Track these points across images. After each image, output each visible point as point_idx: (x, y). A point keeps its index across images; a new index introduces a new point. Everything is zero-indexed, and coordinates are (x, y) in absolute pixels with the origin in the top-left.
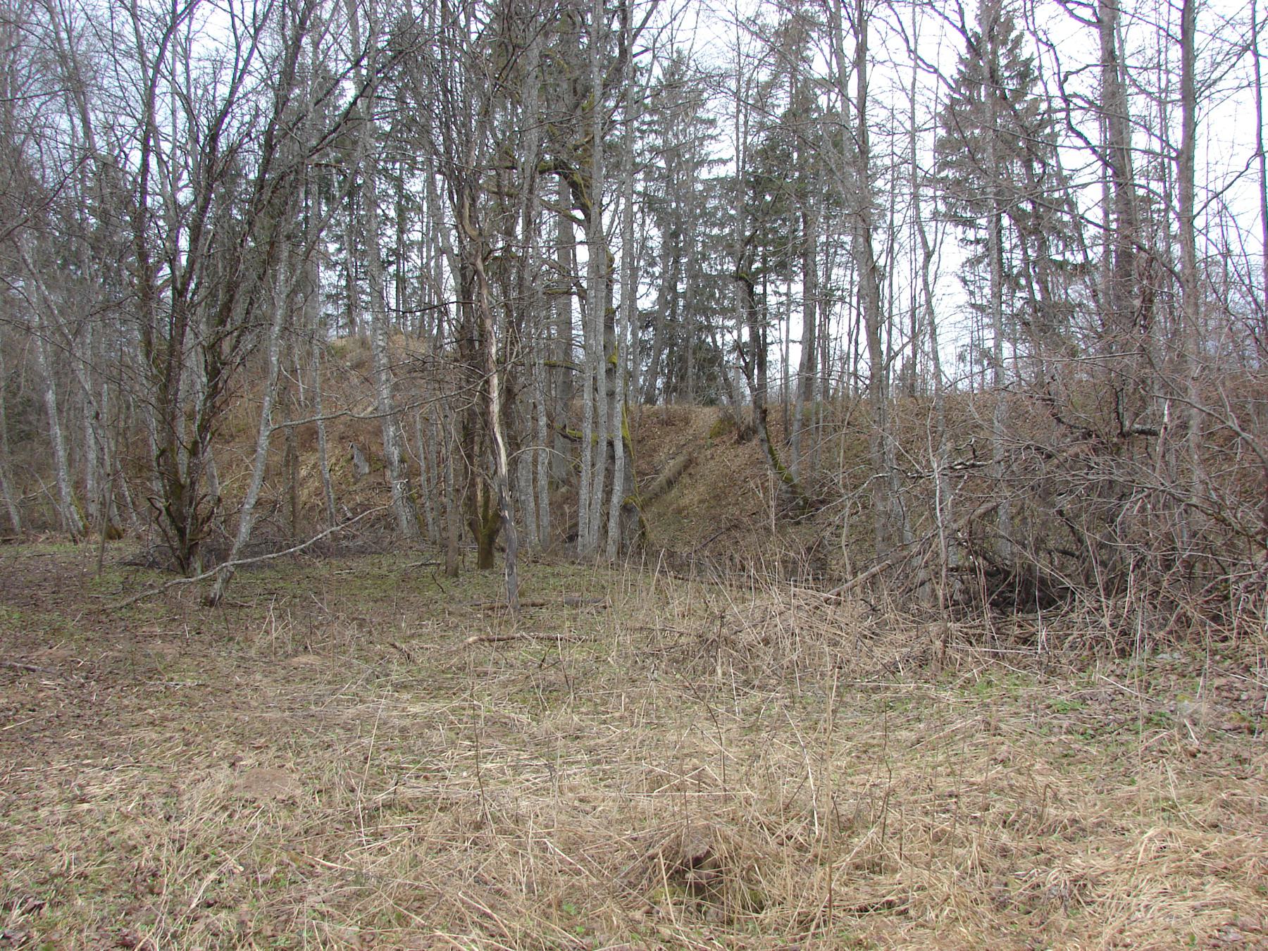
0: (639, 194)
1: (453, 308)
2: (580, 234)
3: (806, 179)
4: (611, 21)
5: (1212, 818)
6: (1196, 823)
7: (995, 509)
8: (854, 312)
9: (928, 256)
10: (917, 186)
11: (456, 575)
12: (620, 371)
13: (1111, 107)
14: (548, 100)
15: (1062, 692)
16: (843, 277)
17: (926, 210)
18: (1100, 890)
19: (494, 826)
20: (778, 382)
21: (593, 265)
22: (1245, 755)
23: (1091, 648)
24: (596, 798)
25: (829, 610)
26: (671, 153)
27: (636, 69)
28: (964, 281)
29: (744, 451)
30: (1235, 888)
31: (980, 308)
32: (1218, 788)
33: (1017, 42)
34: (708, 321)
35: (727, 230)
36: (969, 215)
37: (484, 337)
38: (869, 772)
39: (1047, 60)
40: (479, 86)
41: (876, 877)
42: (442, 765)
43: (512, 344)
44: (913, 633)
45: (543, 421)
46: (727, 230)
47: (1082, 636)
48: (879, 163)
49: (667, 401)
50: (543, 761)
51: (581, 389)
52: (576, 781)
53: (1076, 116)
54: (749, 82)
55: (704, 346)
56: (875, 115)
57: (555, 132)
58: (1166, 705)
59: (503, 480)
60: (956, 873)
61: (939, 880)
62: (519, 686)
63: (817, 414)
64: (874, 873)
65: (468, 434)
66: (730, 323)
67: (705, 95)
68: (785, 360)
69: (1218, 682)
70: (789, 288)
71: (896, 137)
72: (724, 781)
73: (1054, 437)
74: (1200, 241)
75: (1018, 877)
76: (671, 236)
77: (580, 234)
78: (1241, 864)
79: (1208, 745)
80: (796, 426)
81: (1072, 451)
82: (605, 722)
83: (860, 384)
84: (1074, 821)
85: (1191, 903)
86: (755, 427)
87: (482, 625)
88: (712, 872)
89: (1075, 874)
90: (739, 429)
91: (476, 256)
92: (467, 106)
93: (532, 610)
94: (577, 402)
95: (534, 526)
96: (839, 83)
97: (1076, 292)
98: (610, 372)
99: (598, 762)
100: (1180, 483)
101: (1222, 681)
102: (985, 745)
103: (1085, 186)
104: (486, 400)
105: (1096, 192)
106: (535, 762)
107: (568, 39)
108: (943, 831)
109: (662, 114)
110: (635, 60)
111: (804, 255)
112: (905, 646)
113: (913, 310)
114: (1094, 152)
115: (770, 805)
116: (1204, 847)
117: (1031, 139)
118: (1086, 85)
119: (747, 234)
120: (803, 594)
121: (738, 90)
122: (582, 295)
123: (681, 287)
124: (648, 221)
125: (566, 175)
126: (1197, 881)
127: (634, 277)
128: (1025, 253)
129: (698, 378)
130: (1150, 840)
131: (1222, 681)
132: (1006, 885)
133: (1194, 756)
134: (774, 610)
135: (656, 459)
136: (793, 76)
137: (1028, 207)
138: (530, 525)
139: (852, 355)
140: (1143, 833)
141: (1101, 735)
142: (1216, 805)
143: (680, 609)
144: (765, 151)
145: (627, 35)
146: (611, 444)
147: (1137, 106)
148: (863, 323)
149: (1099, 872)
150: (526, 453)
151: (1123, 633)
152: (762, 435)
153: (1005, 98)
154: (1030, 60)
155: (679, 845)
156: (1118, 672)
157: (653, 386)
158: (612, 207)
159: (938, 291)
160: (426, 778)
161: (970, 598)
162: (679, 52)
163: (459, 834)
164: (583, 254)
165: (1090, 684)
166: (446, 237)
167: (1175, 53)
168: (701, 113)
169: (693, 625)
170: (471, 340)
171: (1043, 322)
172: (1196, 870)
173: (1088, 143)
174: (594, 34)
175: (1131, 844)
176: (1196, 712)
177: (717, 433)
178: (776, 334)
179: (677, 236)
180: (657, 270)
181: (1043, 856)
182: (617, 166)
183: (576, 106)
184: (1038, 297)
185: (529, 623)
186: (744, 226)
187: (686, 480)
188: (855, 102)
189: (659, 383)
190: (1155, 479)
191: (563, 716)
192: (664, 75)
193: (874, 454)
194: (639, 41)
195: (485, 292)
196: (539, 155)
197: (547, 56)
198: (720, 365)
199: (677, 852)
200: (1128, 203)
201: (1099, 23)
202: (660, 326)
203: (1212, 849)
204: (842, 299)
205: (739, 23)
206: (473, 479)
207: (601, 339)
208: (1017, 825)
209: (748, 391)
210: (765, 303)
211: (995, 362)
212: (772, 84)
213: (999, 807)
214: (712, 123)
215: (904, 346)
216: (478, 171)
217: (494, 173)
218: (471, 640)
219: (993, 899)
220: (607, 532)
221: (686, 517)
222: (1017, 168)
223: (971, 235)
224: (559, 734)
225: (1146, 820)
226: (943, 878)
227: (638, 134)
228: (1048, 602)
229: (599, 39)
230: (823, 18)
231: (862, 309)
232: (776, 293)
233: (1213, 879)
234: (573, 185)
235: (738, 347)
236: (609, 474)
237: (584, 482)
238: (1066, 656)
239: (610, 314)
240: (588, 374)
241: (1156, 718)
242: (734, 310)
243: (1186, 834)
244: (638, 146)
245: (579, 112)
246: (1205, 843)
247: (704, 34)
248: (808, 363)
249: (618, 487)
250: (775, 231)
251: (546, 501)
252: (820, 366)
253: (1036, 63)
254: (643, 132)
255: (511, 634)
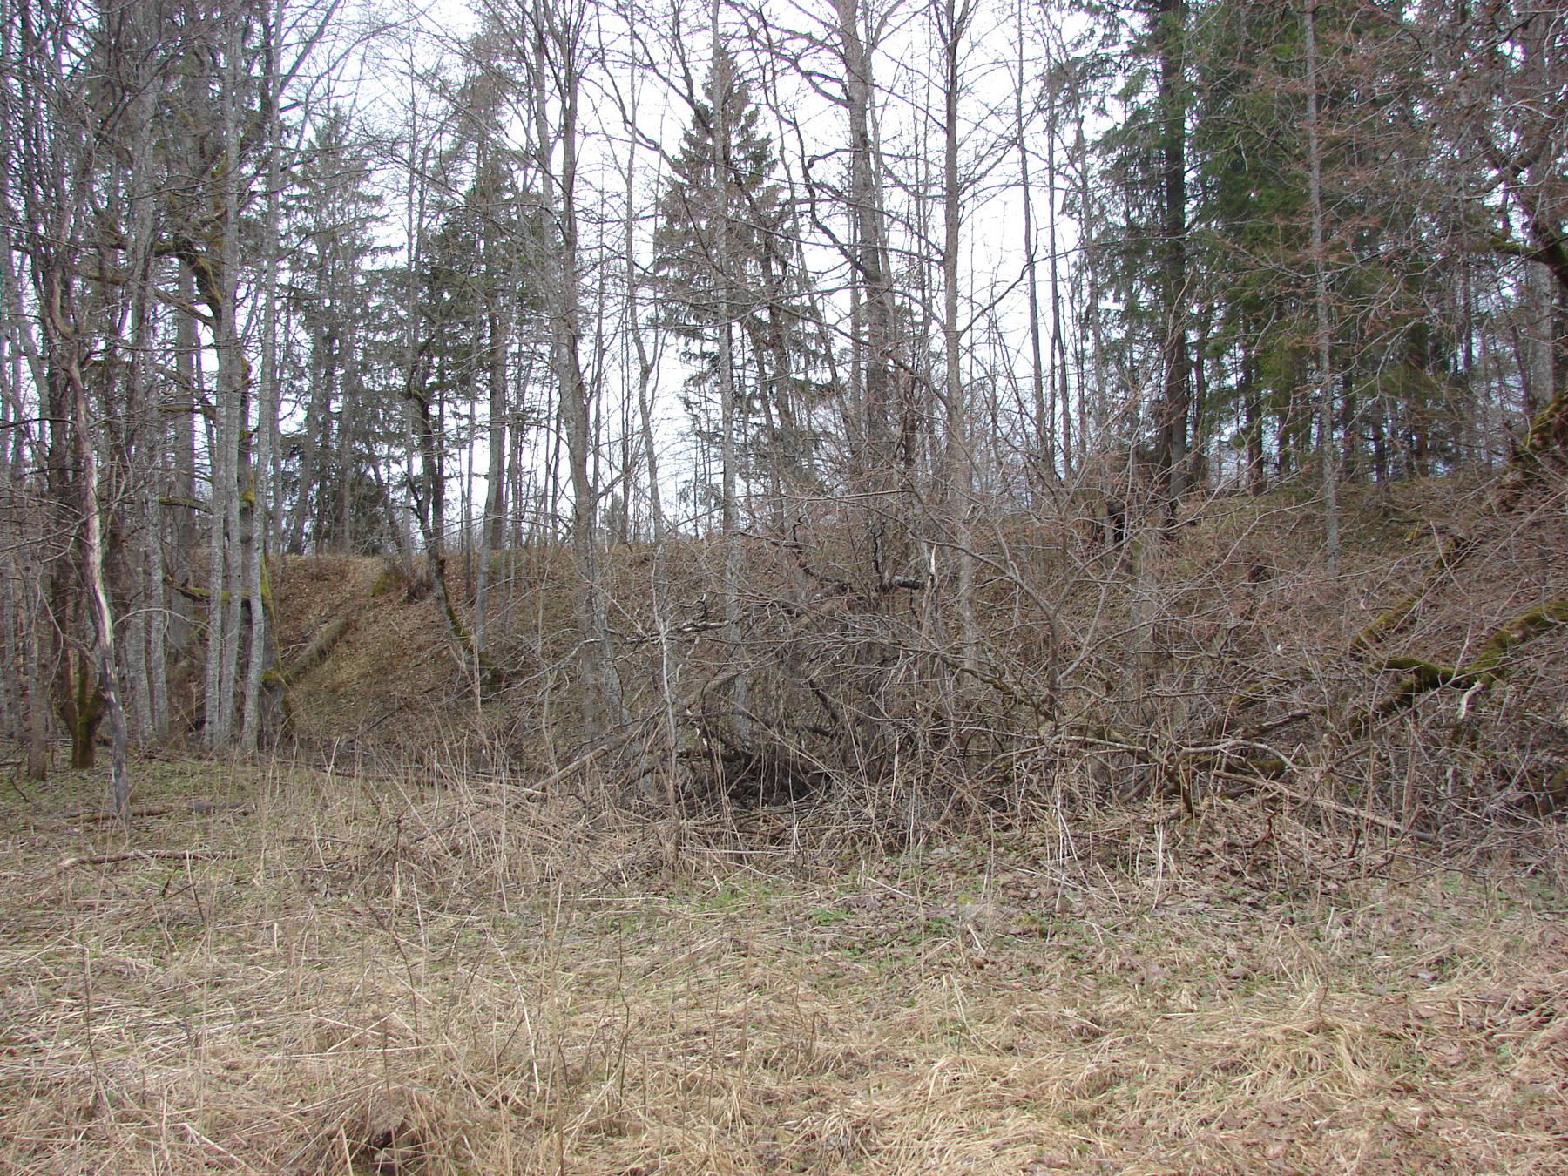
0: (282, 287)
1: (35, 427)
2: (206, 335)
3: (495, 273)
4: (250, 65)
5: (1005, 1040)
6: (989, 1046)
7: (730, 681)
8: (553, 436)
9: (646, 372)
10: (633, 286)
11: (43, 778)
12: (259, 511)
13: (862, 197)
14: (168, 162)
15: (821, 899)
16: (541, 396)
17: (644, 313)
18: (887, 1135)
19: (113, 1113)
20: (457, 527)
21: (224, 376)
22: (1039, 962)
23: (854, 844)
24: (248, 1063)
25: (533, 809)
26: (325, 236)
27: (283, 128)
28: (687, 403)
29: (416, 613)
30: (1039, 1119)
31: (709, 437)
32: (1011, 1003)
33: (752, 119)
34: (370, 449)
35: (394, 336)
36: (693, 322)
37: (80, 469)
38: (593, 1009)
39: (791, 141)
40: (74, 138)
41: (617, 1141)
42: (34, 1033)
43: (119, 475)
44: (638, 834)
45: (158, 575)
46: (394, 336)
47: (843, 831)
48: (586, 257)
49: (318, 550)
50: (173, 1019)
51: (207, 534)
52: (224, 1041)
53: (823, 209)
54: (427, 150)
55: (365, 481)
56: (584, 197)
57: (177, 204)
58: (946, 909)
59: (108, 652)
60: (714, 1128)
61: (694, 1139)
62: (135, 921)
63: (508, 565)
64: (612, 1135)
65: (58, 591)
66: (398, 453)
67: (371, 165)
68: (467, 498)
69: (1004, 878)
70: (472, 409)
71: (606, 226)
72: (415, 1030)
73: (805, 592)
74: (965, 362)
75: (788, 1128)
76: (324, 341)
77: (206, 335)
78: (1043, 1091)
79: (996, 954)
80: (481, 580)
81: (826, 607)
82: (252, 963)
83: (560, 526)
84: (849, 1055)
85: (991, 1141)
86: (433, 581)
87: (82, 841)
88: (408, 1150)
89: (856, 1118)
90: (409, 584)
91: (70, 361)
92: (57, 163)
93: (149, 820)
94: (202, 551)
95: (147, 711)
96: (543, 158)
97: (824, 417)
98: (246, 512)
99: (248, 1015)
100: (950, 649)
101: (1008, 877)
102: (735, 969)
103: (830, 292)
104: (82, 545)
105: (843, 300)
106: (163, 1021)
107: (194, 86)
108: (693, 1079)
109: (314, 187)
110: (282, 116)
111: (492, 368)
112: (628, 851)
113: (625, 440)
114: (843, 252)
115: (477, 1058)
116: (1001, 1074)
117: (768, 234)
118: (832, 172)
119: (421, 340)
120: (503, 790)
121: (412, 159)
122: (210, 413)
123: (335, 406)
124: (293, 323)
125: (189, 260)
126: (996, 1115)
127: (276, 389)
128: (762, 370)
129: (357, 521)
130: (941, 1071)
131: (1008, 877)
132: (775, 1138)
133: (981, 967)
134: (465, 811)
135: (304, 624)
136: (481, 146)
137: (765, 316)
138: (141, 710)
139: (550, 493)
140: (930, 1063)
141: (872, 948)
142: (1010, 1024)
143: (338, 811)
144: (444, 238)
145: (272, 83)
146: (247, 604)
147: (895, 200)
148: (564, 450)
149: (884, 1114)
150: (136, 616)
151: (891, 826)
152: (439, 591)
153: (740, 184)
154: (767, 140)
155: (364, 1118)
156: (887, 872)
157: (299, 529)
158: (249, 302)
159: (656, 413)
160: (12, 1053)
161: (707, 789)
162: (336, 109)
163: (63, 1126)
164: (210, 361)
165: (855, 888)
166: (26, 332)
167: (938, 141)
168: (364, 188)
169: (357, 834)
170: (62, 470)
171: (783, 452)
172: (993, 1102)
173: (835, 241)
174: (229, 80)
175: (918, 1078)
176: (980, 915)
177: (382, 590)
178: (456, 465)
179: (332, 341)
180: (306, 384)
181: (815, 1100)
182: (256, 250)
183: (204, 171)
184: (777, 422)
185: (145, 837)
186: (416, 330)
187: (342, 649)
188: (560, 180)
189: (308, 527)
190: (924, 639)
191: (203, 957)
192: (318, 137)
193: (580, 614)
194: (287, 92)
195: (82, 407)
196: (155, 230)
197: (166, 104)
198: (385, 504)
199: (362, 1127)
200: (884, 312)
201: (849, 102)
202: (309, 454)
203: (1011, 1076)
204: (538, 423)
205: (415, 77)
206: (65, 652)
207: (234, 470)
208: (781, 1065)
209: (420, 537)
210: (441, 427)
211: (726, 503)
212: (457, 154)
213: (758, 1043)
214: (378, 200)
215: (613, 483)
216: (74, 247)
217: (92, 251)
218: (67, 862)
219: (760, 1157)
220: (242, 716)
221: (344, 695)
222: (752, 268)
223: (695, 347)
224: (193, 982)
225: (931, 1047)
226: (698, 1135)
227: (282, 211)
228: (801, 790)
229: (235, 86)
230: (521, 77)
231: (564, 434)
232: (456, 414)
233: (1013, 1110)
234: (201, 273)
235: (409, 482)
236: (245, 642)
237: (213, 655)
238: (821, 855)
239: (245, 439)
240: (219, 514)
241: (935, 925)
242: (402, 435)
243: (982, 1061)
244: (283, 225)
245: (207, 179)
246: (1002, 1069)
247: (370, 88)
248: (496, 503)
249: (257, 658)
250: (454, 337)
251: (163, 678)
252: (510, 506)
253: (776, 145)
254: (289, 209)
255: (121, 852)
